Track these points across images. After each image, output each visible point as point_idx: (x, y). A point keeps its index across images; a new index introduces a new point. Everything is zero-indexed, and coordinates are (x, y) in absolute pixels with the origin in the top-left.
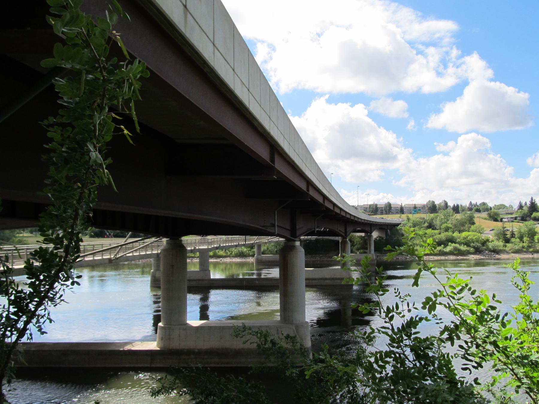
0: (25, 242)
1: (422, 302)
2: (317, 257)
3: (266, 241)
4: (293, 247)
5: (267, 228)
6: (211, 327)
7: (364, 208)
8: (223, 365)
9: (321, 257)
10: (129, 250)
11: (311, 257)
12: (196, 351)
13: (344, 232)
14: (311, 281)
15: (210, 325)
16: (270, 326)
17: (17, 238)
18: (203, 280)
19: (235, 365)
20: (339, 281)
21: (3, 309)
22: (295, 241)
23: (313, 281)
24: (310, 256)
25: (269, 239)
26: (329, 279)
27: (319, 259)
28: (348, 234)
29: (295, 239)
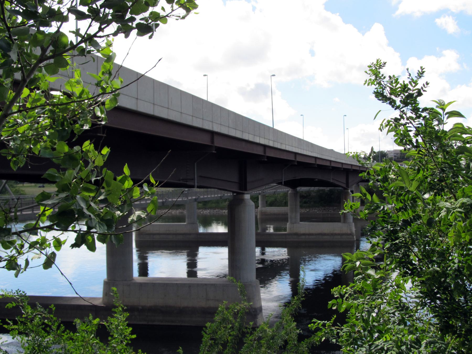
0: (22, 192)
1: (70, 245)
2: (330, 209)
3: (260, 192)
4: (242, 200)
5: (187, 182)
6: (155, 284)
7: (395, 153)
8: (167, 324)
9: (335, 209)
10: (26, 205)
11: (324, 210)
12: (140, 308)
13: (345, 183)
14: (307, 236)
15: (154, 282)
16: (216, 284)
17: (15, 188)
18: (190, 234)
19: (179, 324)
20: (339, 237)
21: (344, 298)
22: (243, 194)
23: (303, 237)
24: (323, 208)
25: (263, 189)
26: (339, 234)
27: (332, 212)
28: (350, 185)
29: (243, 192)
